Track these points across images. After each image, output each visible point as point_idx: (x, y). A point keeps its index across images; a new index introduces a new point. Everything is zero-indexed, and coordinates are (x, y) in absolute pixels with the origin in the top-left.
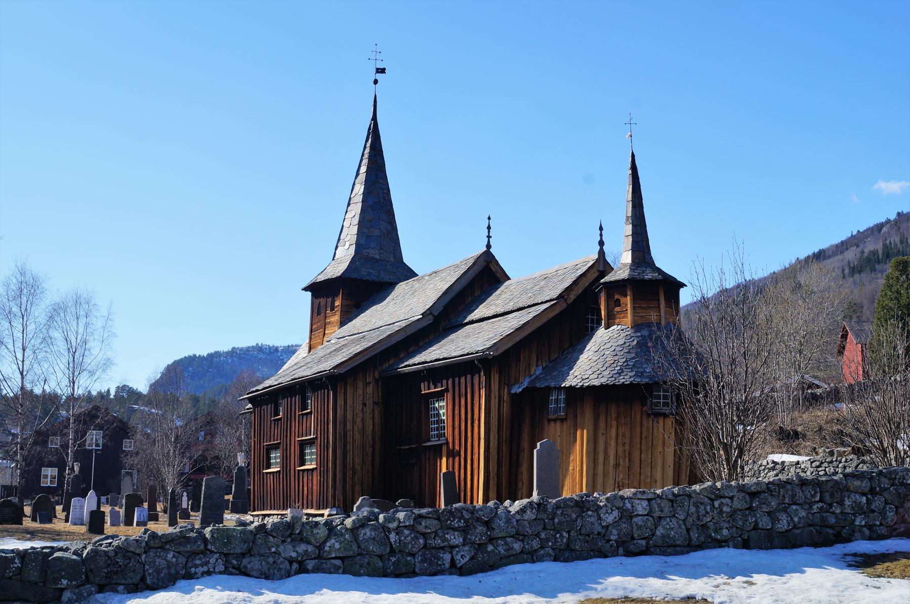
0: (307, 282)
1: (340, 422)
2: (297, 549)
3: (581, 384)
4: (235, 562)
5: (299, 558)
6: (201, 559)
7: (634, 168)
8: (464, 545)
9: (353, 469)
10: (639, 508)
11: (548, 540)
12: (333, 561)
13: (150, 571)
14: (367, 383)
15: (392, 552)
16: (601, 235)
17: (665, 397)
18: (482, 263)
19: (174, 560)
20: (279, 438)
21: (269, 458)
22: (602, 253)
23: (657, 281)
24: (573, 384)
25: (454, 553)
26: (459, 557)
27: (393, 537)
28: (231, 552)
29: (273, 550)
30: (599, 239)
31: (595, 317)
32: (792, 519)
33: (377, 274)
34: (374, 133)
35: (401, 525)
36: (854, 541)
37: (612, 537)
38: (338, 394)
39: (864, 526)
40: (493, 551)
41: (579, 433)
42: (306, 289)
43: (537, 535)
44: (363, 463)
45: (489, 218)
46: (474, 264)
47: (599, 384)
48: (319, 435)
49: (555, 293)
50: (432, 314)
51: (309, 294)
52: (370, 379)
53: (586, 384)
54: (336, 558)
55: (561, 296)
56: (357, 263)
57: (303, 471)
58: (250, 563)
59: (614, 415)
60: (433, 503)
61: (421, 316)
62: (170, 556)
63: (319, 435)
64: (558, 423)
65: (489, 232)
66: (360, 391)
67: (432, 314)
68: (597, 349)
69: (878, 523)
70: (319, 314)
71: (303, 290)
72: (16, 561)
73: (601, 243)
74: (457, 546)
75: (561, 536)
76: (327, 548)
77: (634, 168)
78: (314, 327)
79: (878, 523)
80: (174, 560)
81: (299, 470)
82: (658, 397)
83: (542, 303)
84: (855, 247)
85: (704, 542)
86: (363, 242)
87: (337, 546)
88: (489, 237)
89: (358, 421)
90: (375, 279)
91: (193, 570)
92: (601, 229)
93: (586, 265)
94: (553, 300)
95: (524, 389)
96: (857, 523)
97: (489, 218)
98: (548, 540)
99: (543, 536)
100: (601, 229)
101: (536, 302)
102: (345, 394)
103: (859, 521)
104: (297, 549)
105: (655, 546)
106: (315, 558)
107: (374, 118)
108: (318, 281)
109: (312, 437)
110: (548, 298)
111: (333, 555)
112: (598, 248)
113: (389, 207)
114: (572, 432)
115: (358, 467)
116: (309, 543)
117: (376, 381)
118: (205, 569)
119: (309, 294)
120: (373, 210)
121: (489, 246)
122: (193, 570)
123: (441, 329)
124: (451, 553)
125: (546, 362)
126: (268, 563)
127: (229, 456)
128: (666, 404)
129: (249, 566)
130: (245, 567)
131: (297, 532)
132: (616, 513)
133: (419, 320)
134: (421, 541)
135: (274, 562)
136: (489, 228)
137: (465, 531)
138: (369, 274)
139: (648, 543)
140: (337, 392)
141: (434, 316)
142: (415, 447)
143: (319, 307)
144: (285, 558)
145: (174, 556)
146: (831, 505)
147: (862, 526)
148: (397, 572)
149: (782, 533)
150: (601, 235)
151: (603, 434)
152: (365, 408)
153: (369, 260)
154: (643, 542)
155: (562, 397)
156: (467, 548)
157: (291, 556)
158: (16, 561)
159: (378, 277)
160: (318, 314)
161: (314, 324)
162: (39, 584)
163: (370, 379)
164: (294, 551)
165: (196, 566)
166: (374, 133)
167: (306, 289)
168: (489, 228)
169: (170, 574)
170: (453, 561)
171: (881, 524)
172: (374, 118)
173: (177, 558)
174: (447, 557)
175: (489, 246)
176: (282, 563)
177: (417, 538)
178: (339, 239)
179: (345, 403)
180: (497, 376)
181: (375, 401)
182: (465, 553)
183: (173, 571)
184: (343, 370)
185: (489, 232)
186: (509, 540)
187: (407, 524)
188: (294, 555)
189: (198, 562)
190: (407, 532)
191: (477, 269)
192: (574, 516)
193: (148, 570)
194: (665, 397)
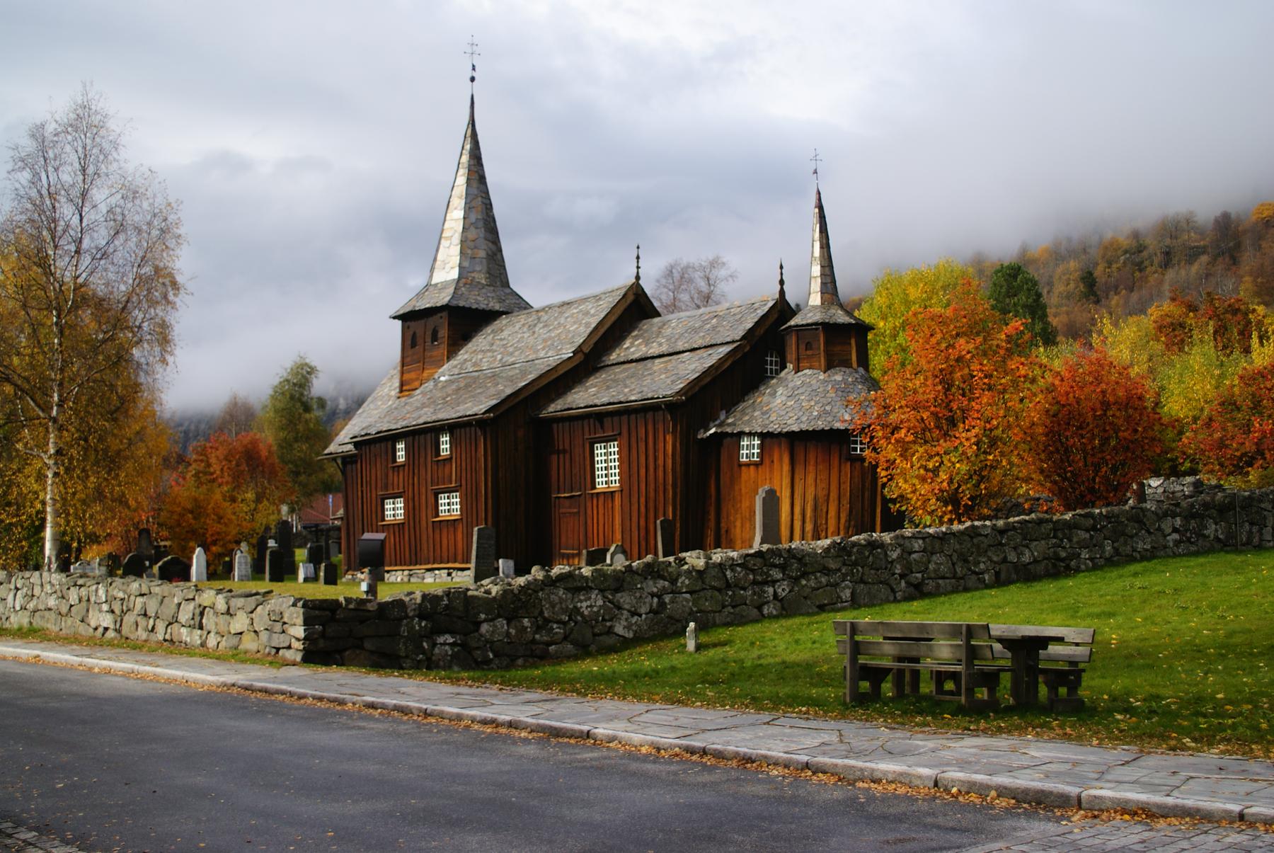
0: (401, 302)
2: (657, 585)
3: (779, 430)
4: (610, 597)
6: (584, 595)
7: (820, 207)
8: (783, 580)
10: (916, 546)
11: (846, 575)
12: (684, 595)
13: (547, 606)
15: (728, 586)
16: (782, 274)
18: (631, 298)
19: (564, 596)
20: (401, 485)
22: (782, 292)
23: (850, 324)
24: (771, 430)
25: (776, 586)
26: (780, 590)
27: (728, 573)
29: (639, 586)
30: (779, 278)
31: (774, 359)
32: (1033, 554)
33: (486, 302)
35: (735, 563)
36: (1078, 570)
37: (897, 571)
39: (1088, 559)
40: (806, 585)
43: (839, 570)
45: (638, 248)
46: (624, 296)
47: (799, 430)
48: (463, 482)
49: (739, 333)
51: (399, 323)
53: (785, 430)
54: (686, 593)
56: (463, 289)
57: (384, 525)
58: (622, 597)
59: (812, 462)
60: (588, 552)
61: (572, 355)
62: (561, 593)
63: (463, 482)
64: (752, 468)
65: (638, 262)
68: (790, 394)
69: (1098, 556)
70: (414, 345)
71: (390, 317)
72: (445, 599)
73: (782, 282)
74: (778, 581)
75: (858, 570)
76: (679, 584)
77: (820, 207)
78: (408, 360)
79: (1098, 556)
80: (564, 596)
81: (433, 522)
84: (1252, 406)
85: (965, 575)
86: (466, 264)
87: (687, 582)
88: (638, 267)
90: (484, 307)
91: (579, 605)
92: (781, 267)
93: (765, 305)
96: (1082, 556)
97: (638, 248)
98: (846, 575)
99: (843, 571)
100: (781, 267)
101: (713, 342)
103: (1085, 554)
104: (657, 585)
105: (928, 579)
106: (670, 593)
107: (472, 122)
108: (417, 309)
109: (453, 485)
110: (729, 339)
111: (684, 590)
112: (779, 287)
113: (492, 224)
114: (768, 477)
116: (665, 579)
118: (588, 603)
120: (477, 228)
121: (638, 278)
122: (579, 605)
124: (774, 587)
126: (636, 598)
129: (622, 600)
130: (618, 601)
131: (656, 570)
132: (899, 551)
133: (570, 358)
134: (751, 577)
135: (641, 597)
136: (638, 258)
137: (783, 568)
139: (923, 576)
143: (414, 336)
144: (649, 593)
145: (564, 593)
146: (1062, 540)
147: (1086, 559)
148: (733, 604)
149: (1025, 565)
150: (782, 274)
153: (472, 284)
154: (919, 575)
155: (757, 442)
156: (785, 583)
158: (445, 599)
159: (487, 305)
160: (410, 343)
161: (408, 356)
165: (581, 601)
168: (638, 258)
169: (562, 608)
170: (775, 593)
171: (1100, 558)
172: (472, 122)
173: (566, 594)
174: (771, 590)
175: (638, 278)
176: (646, 597)
177: (748, 574)
178: (435, 260)
182: (785, 587)
183: (564, 606)
185: (638, 262)
186: (818, 574)
187: (740, 562)
188: (655, 590)
189: (582, 598)
190: (739, 569)
192: (867, 554)
193: (544, 606)
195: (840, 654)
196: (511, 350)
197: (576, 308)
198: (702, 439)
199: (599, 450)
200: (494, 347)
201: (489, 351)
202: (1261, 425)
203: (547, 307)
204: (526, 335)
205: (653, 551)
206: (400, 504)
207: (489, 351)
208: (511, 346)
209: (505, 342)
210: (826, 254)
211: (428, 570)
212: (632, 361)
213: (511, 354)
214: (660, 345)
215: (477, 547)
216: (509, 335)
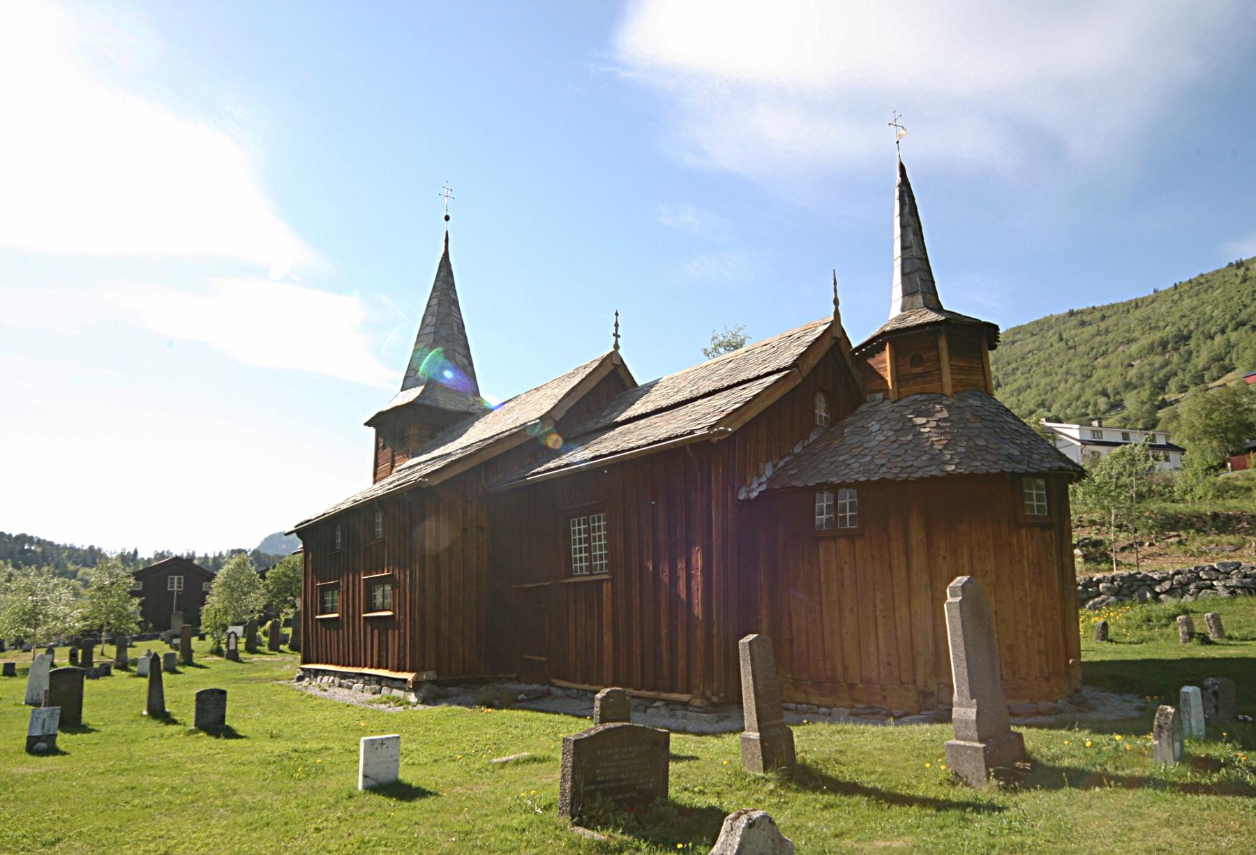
21: (323, 602)
34: (445, 262)
41: (390, 632)
42: (368, 424)
45: (617, 314)
50: (553, 419)
55: (795, 364)
64: (843, 544)
71: (366, 424)
83: (759, 377)
94: (784, 369)
95: (761, 492)
97: (617, 314)
107: (446, 255)
121: (616, 346)
136: (617, 325)
142: (549, 585)
151: (944, 557)
162: (1214, 314)
166: (445, 262)
167: (368, 424)
172: (446, 255)
175: (616, 346)
184: (435, 482)
191: (604, 372)
198: (748, 500)
199: (577, 528)
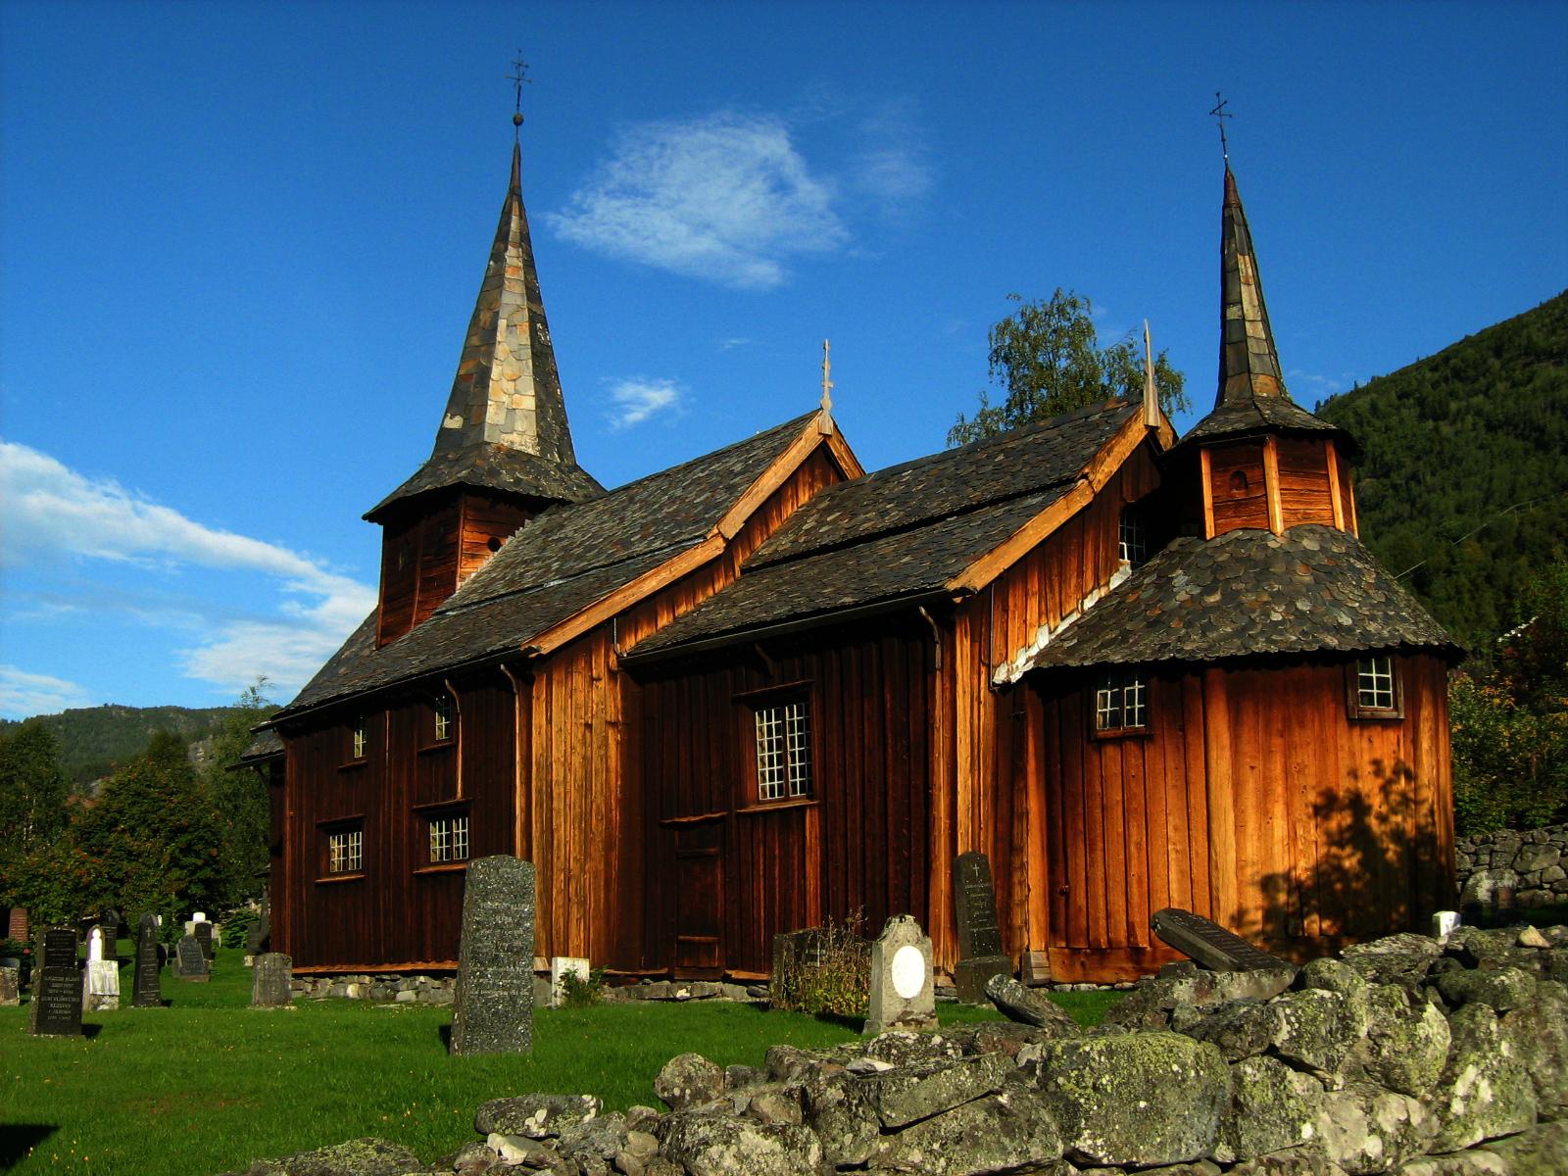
0: (379, 494)
1: (538, 764)
5: (1389, 1162)
9: (567, 871)
14: (592, 679)
17: (1382, 683)
28: (1166, 1158)
38: (534, 701)
42: (370, 517)
44: (587, 854)
50: (723, 536)
52: (599, 668)
64: (1132, 748)
66: (580, 697)
67: (723, 536)
82: (1368, 682)
89: (577, 760)
102: (549, 703)
115: (575, 871)
117: (612, 674)
119: (378, 530)
123: (737, 569)
125: (1055, 618)
127: (1365, 591)
128: (1383, 700)
138: (518, 481)
140: (531, 697)
141: (725, 540)
152: (588, 734)
157: (1364, 1156)
163: (599, 668)
164: (1372, 1131)
167: (370, 517)
179: (549, 721)
180: (967, 643)
181: (609, 719)
194: (1382, 683)
195: (1212, 1109)
196: (578, 551)
197: (702, 471)
199: (764, 724)
200: (547, 553)
201: (537, 559)
202: (489, 928)
203: (646, 479)
204: (607, 526)
205: (1064, 934)
206: (356, 841)
207: (537, 559)
208: (578, 546)
209: (565, 543)
210: (1255, 296)
211: (406, 974)
212: (824, 549)
213: (579, 558)
214: (883, 514)
215: (305, 966)
216: (575, 531)
